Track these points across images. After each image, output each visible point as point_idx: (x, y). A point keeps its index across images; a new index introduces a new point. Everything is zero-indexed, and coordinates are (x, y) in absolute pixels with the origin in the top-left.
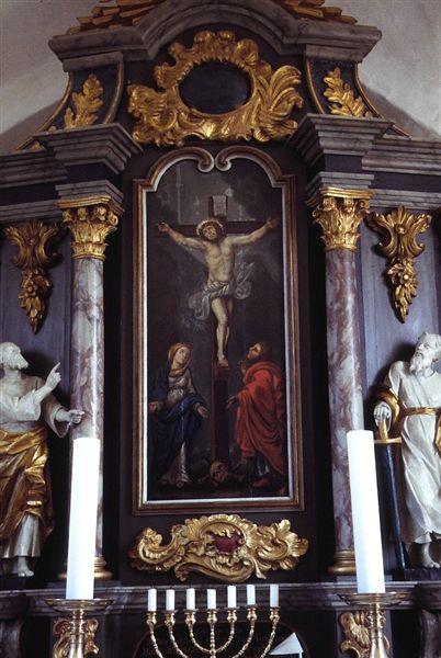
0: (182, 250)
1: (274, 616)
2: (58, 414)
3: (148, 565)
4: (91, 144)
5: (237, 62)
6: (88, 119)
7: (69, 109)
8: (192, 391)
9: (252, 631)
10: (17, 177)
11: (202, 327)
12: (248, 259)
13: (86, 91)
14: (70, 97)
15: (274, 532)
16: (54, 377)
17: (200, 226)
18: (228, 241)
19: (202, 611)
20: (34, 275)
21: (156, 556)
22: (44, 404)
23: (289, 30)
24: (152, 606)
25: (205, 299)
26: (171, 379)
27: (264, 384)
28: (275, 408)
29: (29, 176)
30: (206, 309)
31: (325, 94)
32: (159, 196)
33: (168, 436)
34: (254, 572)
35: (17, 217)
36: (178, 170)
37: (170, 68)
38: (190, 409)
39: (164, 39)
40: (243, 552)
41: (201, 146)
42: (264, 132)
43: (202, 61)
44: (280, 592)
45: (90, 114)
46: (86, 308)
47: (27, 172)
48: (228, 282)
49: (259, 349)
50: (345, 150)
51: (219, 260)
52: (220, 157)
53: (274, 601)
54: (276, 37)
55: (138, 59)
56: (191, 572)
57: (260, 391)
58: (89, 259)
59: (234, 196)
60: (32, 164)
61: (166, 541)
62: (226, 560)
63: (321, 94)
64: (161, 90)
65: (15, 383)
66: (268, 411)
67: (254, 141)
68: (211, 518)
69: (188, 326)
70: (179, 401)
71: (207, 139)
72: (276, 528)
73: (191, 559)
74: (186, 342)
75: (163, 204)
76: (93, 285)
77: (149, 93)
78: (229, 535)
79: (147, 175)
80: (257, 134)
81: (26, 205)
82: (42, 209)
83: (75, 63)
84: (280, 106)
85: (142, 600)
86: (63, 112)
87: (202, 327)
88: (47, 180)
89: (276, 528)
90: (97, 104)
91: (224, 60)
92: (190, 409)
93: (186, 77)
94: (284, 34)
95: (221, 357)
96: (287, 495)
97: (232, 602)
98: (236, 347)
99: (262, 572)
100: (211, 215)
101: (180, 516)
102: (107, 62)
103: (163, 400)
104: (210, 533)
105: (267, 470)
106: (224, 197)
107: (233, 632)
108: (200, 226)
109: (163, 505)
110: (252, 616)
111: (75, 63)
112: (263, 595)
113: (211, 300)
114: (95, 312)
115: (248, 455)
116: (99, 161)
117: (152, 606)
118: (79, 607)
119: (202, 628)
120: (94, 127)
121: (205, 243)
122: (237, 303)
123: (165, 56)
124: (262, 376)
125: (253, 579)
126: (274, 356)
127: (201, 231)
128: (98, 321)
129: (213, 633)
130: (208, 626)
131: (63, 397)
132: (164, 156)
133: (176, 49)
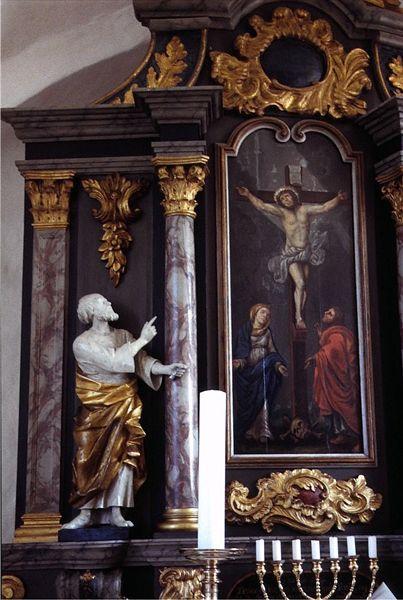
0: (260, 214)
1: (374, 567)
2: (152, 366)
3: (238, 516)
4: (191, 105)
5: (315, 40)
6: (171, 80)
7: (151, 69)
8: (273, 350)
9: (354, 581)
10: (97, 130)
11: (281, 290)
12: (321, 228)
13: (169, 52)
14: (153, 56)
15: (351, 487)
16: (149, 331)
17: (277, 194)
18: (304, 209)
19: (308, 562)
20: (118, 229)
21: (247, 508)
22: (136, 358)
23: (362, 15)
24: (261, 556)
25: (283, 263)
26: (253, 338)
27: (339, 348)
28: (348, 371)
29: (108, 130)
30: (284, 274)
31: (390, 79)
32: (239, 161)
33: (251, 392)
34: (336, 525)
35: (96, 170)
36: (256, 138)
37: (251, 40)
38: (271, 368)
39: (246, 11)
40: (326, 506)
41: (278, 117)
42: (338, 108)
43: (283, 36)
44: (357, 543)
45: (175, 75)
46: (182, 264)
47: (108, 126)
48: (304, 248)
49: (333, 313)
50: (44, 137)
51: (295, 226)
52: (297, 129)
53: (373, 552)
54: (348, 20)
55: (221, 27)
56: (275, 524)
57: (335, 353)
58: (184, 216)
59: (308, 166)
60: (115, 119)
61: (253, 493)
62: (310, 513)
63: (387, 79)
64: (244, 59)
65: (105, 334)
66: (344, 373)
67: (328, 117)
68: (295, 472)
69: (268, 288)
70: (260, 360)
71: (285, 111)
72: (354, 483)
73: (278, 512)
74: (265, 302)
75: (243, 169)
76: (185, 239)
77: (233, 62)
78: (313, 489)
79: (230, 139)
80: (332, 110)
81: (107, 159)
82: (124, 164)
83: (161, 24)
84: (352, 85)
85: (360, 549)
86: (145, 71)
87: (281, 290)
88: (128, 136)
89: (354, 483)
90: (179, 67)
91: (303, 37)
92: (271, 368)
93: (267, 49)
94: (356, 19)
95: (299, 319)
96: (362, 452)
97: (334, 553)
98: (313, 310)
99: (343, 524)
100: (288, 183)
101: (266, 470)
102: (195, 26)
103: (246, 358)
104: (295, 486)
105: (343, 428)
106: (299, 167)
107: (336, 582)
108: (277, 194)
109: (250, 459)
110: (354, 566)
111: (161, 24)
112: (362, 547)
113: (289, 265)
114: (190, 269)
115: (326, 414)
116: (195, 121)
117: (261, 556)
118: (212, 556)
119: (308, 578)
120: (178, 88)
121: (282, 210)
122: (312, 269)
123: (245, 26)
124: (336, 339)
125: (334, 531)
126: (348, 321)
127: (278, 198)
128: (192, 278)
129: (318, 583)
130: (293, 576)
131: (158, 349)
132: (246, 123)
133: (256, 21)
